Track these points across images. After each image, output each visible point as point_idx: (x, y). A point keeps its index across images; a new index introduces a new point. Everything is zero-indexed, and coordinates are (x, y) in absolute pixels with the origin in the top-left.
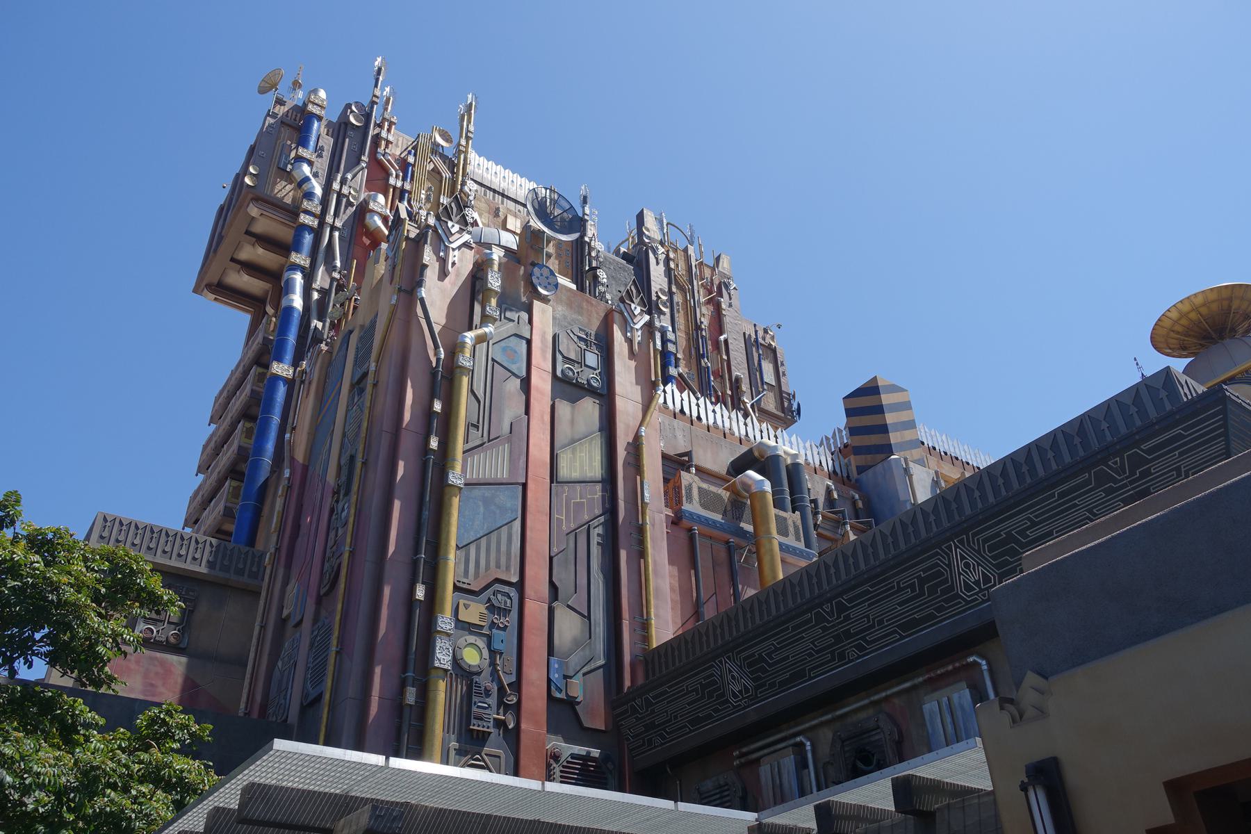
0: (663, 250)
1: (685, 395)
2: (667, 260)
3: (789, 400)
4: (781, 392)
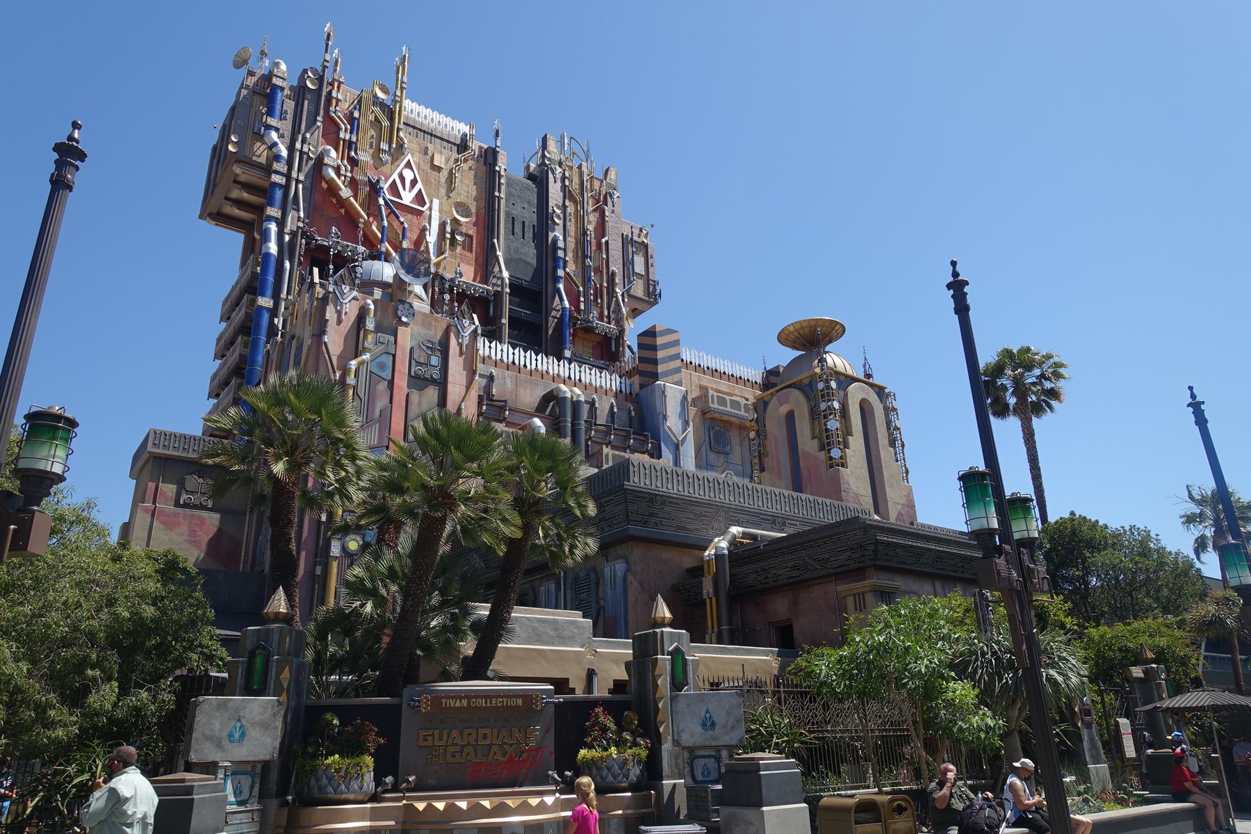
0: (561, 170)
1: (516, 351)
2: (564, 178)
3: (654, 286)
4: (648, 279)
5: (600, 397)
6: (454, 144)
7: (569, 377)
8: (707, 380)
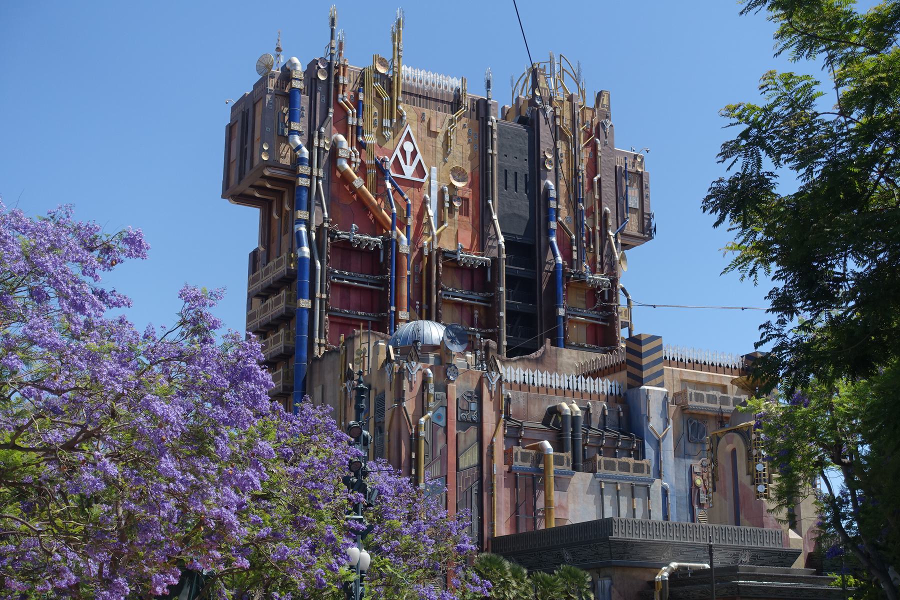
0: (551, 109)
2: (555, 117)
3: (649, 220)
4: (643, 213)
5: (594, 403)
6: (448, 103)
7: (569, 388)
8: (690, 374)
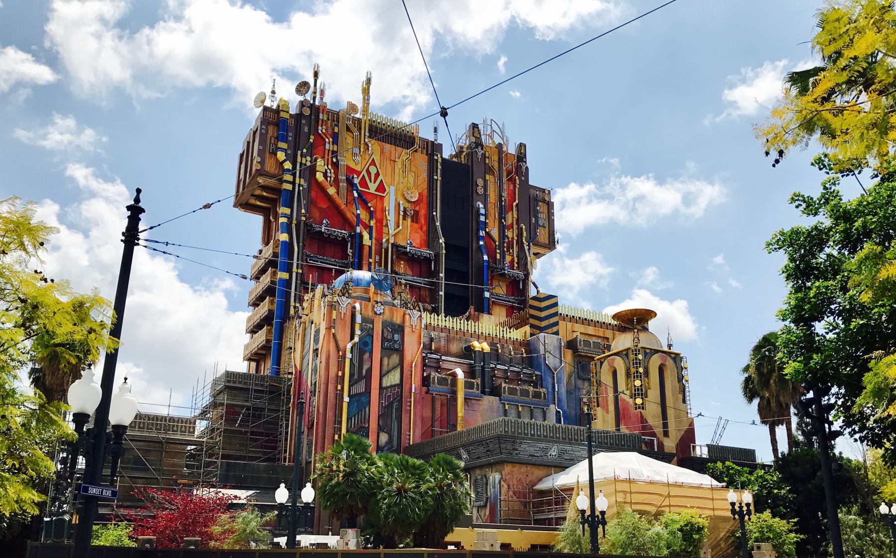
8: (579, 328)
